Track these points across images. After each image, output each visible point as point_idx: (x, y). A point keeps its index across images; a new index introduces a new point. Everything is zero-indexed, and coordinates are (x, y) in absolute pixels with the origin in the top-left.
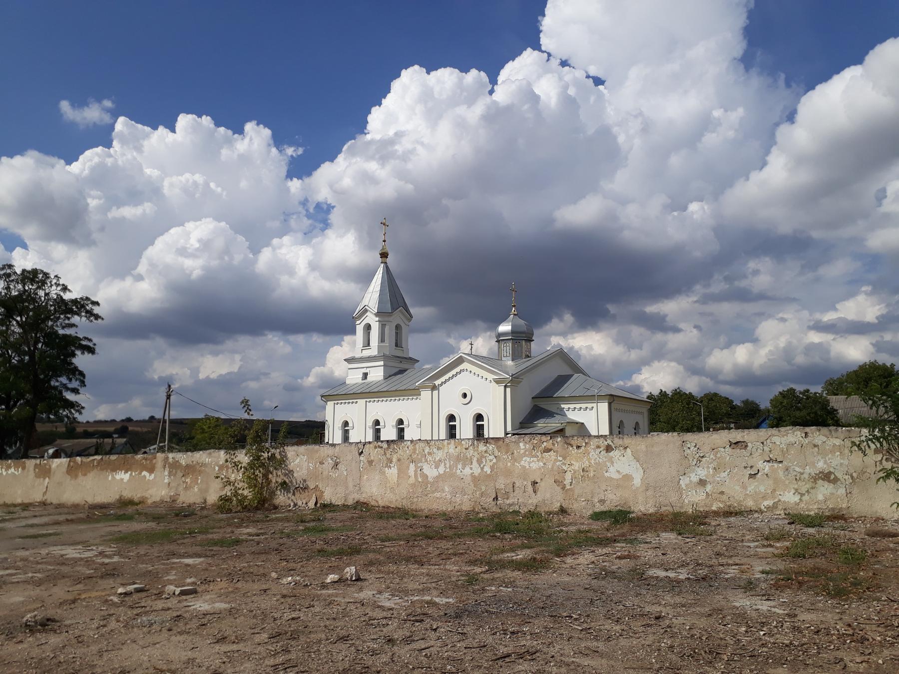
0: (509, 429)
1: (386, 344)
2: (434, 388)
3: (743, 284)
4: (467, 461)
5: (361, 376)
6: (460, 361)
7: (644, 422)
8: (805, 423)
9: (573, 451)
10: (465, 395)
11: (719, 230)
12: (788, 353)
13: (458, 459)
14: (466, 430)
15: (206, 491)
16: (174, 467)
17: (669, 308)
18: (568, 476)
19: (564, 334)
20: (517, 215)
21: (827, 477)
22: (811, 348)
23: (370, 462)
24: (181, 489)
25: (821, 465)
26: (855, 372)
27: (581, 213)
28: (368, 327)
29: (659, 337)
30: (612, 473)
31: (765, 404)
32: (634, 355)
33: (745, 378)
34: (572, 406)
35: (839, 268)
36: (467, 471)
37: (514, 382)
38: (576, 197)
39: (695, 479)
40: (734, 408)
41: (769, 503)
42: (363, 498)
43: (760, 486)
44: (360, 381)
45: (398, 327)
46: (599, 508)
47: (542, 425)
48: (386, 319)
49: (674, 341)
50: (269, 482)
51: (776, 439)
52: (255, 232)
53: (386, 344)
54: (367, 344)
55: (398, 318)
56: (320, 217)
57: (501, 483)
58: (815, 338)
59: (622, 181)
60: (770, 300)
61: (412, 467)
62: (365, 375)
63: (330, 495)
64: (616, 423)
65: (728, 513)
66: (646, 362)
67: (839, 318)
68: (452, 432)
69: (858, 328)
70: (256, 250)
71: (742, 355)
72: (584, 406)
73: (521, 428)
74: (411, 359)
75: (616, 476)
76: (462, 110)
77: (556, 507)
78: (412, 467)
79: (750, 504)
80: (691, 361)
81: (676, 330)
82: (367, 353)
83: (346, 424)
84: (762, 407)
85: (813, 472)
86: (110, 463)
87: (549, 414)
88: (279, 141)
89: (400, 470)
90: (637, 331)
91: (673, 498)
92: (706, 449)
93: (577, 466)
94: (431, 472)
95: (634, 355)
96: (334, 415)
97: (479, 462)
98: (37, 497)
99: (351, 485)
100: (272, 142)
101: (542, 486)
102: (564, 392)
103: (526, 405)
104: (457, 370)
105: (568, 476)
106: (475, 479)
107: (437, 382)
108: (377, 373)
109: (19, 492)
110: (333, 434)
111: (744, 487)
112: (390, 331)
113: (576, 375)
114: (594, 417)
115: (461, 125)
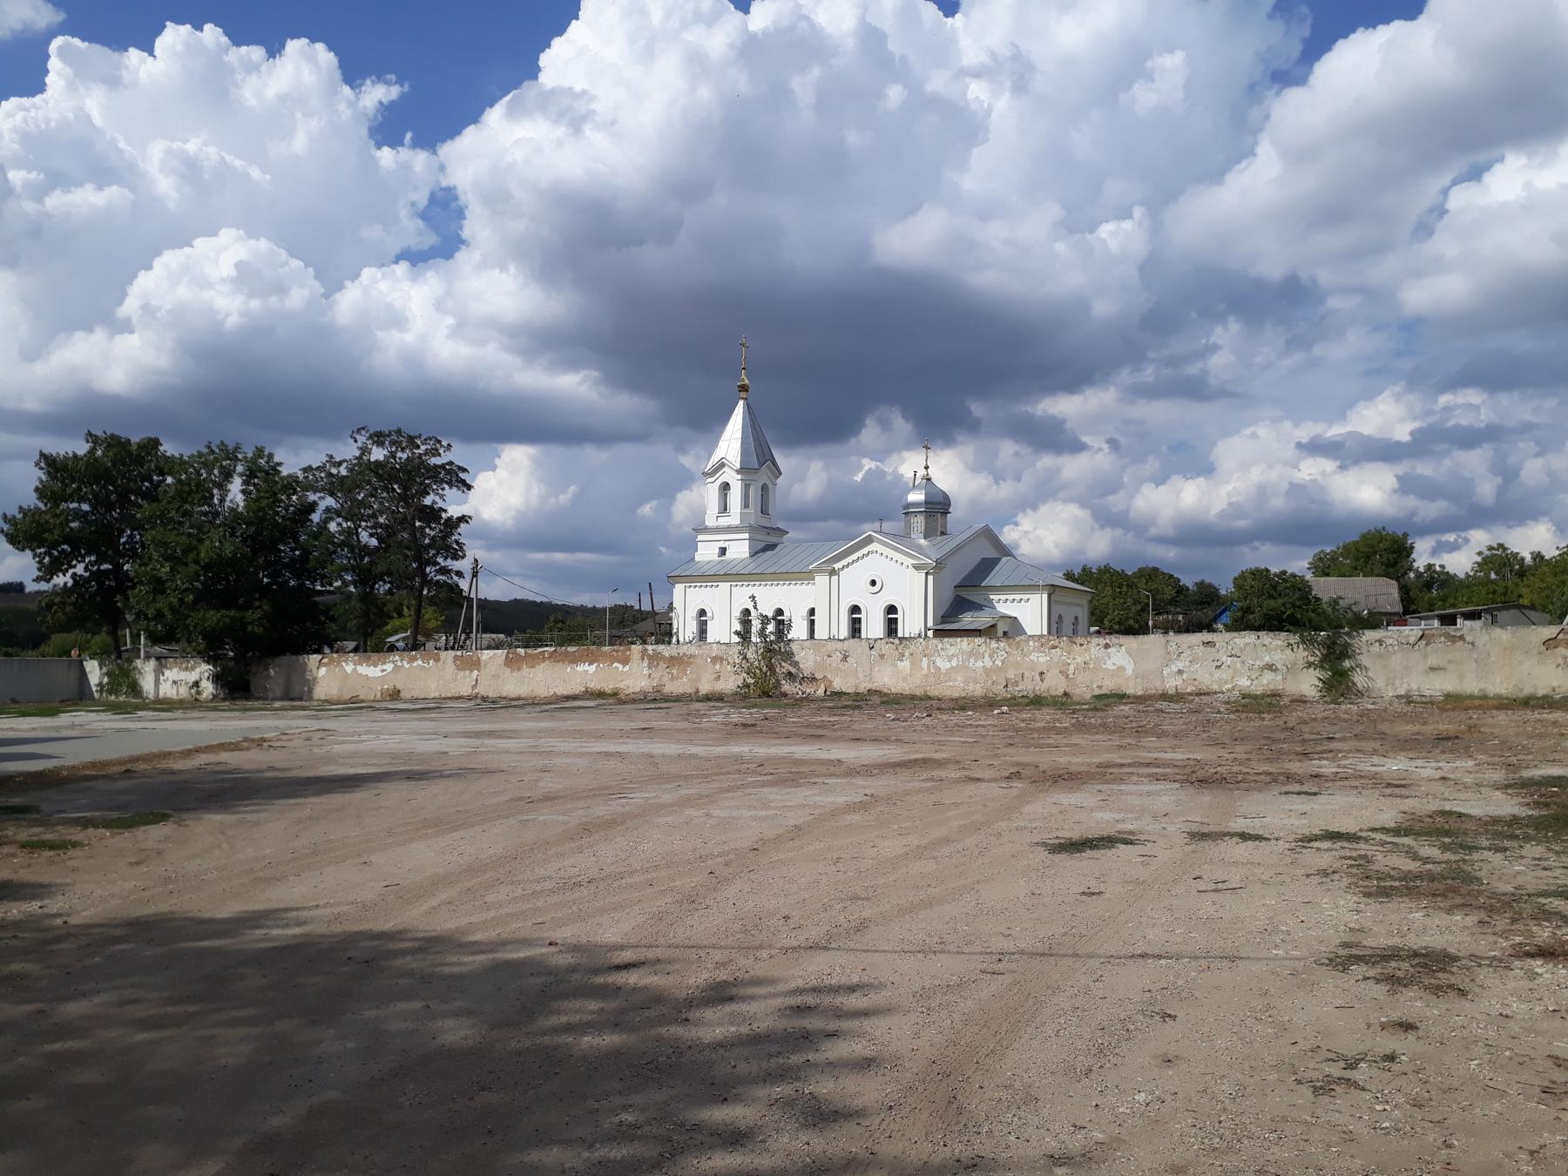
0: (930, 624)
1: (751, 510)
2: (833, 572)
3: (1193, 370)
4: (980, 656)
5: (717, 551)
6: (869, 540)
7: (1083, 615)
8: (1258, 629)
9: (1077, 648)
10: (873, 583)
11: (1150, 266)
12: (1263, 492)
13: (971, 653)
14: (874, 626)
15: (698, 680)
16: (655, 659)
17: (1064, 406)
18: (1072, 668)
19: (881, 455)
20: (806, 239)
21: (1271, 667)
22: (1295, 489)
23: (882, 656)
24: (665, 679)
25: (1267, 659)
26: (1355, 543)
27: (910, 240)
28: (726, 487)
29: (1047, 461)
30: (1109, 665)
31: (1226, 587)
32: (1006, 490)
33: (1195, 534)
34: (1003, 597)
35: (1352, 345)
36: (980, 664)
37: (938, 568)
38: (910, 209)
39: (1175, 669)
40: (1181, 590)
41: (1229, 686)
42: (874, 686)
43: (1223, 674)
44: (716, 558)
45: (764, 488)
46: (1097, 692)
47: (968, 620)
48: (751, 477)
49: (1072, 468)
50: (774, 672)
51: (1237, 641)
52: (328, 252)
53: (751, 510)
54: (724, 509)
55: (764, 476)
56: (440, 230)
57: (1011, 674)
58: (1312, 469)
59: (979, 174)
60: (1231, 397)
61: (925, 660)
62: (723, 551)
63: (838, 684)
64: (1055, 618)
65: (1199, 694)
66: (1028, 505)
67: (1351, 434)
68: (855, 628)
69: (1381, 452)
70: (332, 284)
71: (1189, 498)
72: (1018, 597)
73: (943, 622)
74: (779, 529)
75: (1112, 667)
76: (695, 35)
77: (1060, 692)
78: (925, 660)
79: (1215, 687)
80: (1101, 505)
81: (1077, 447)
82: (724, 521)
83: (702, 613)
84: (1223, 592)
85: (1261, 663)
86: (567, 654)
87: (977, 607)
88: (353, 73)
89: (912, 664)
90: (1008, 449)
91: (1158, 684)
92: (1185, 646)
93: (1079, 659)
94: (944, 665)
95: (1006, 490)
96: (686, 602)
97: (991, 657)
98: (465, 690)
99: (861, 676)
100: (338, 75)
101: (1048, 675)
102: (993, 579)
103: (948, 595)
104: (865, 551)
105: (1072, 668)
106: (987, 671)
107: (837, 566)
108: (740, 549)
109: (434, 686)
110: (685, 627)
111: (1211, 675)
112: (754, 492)
113: (1005, 559)
114: (1030, 612)
115: (697, 63)
